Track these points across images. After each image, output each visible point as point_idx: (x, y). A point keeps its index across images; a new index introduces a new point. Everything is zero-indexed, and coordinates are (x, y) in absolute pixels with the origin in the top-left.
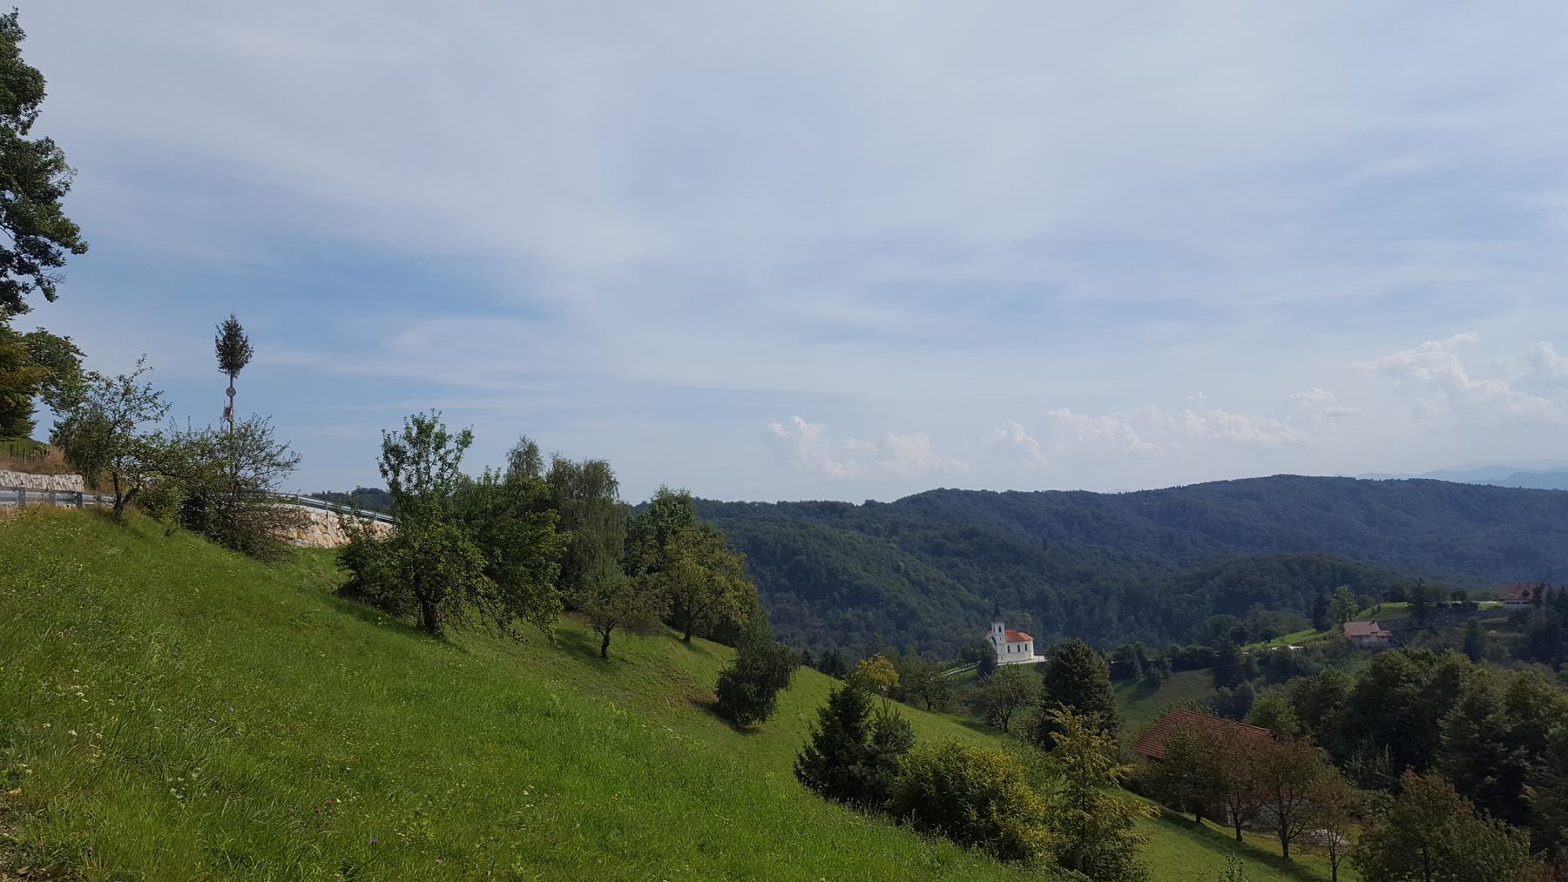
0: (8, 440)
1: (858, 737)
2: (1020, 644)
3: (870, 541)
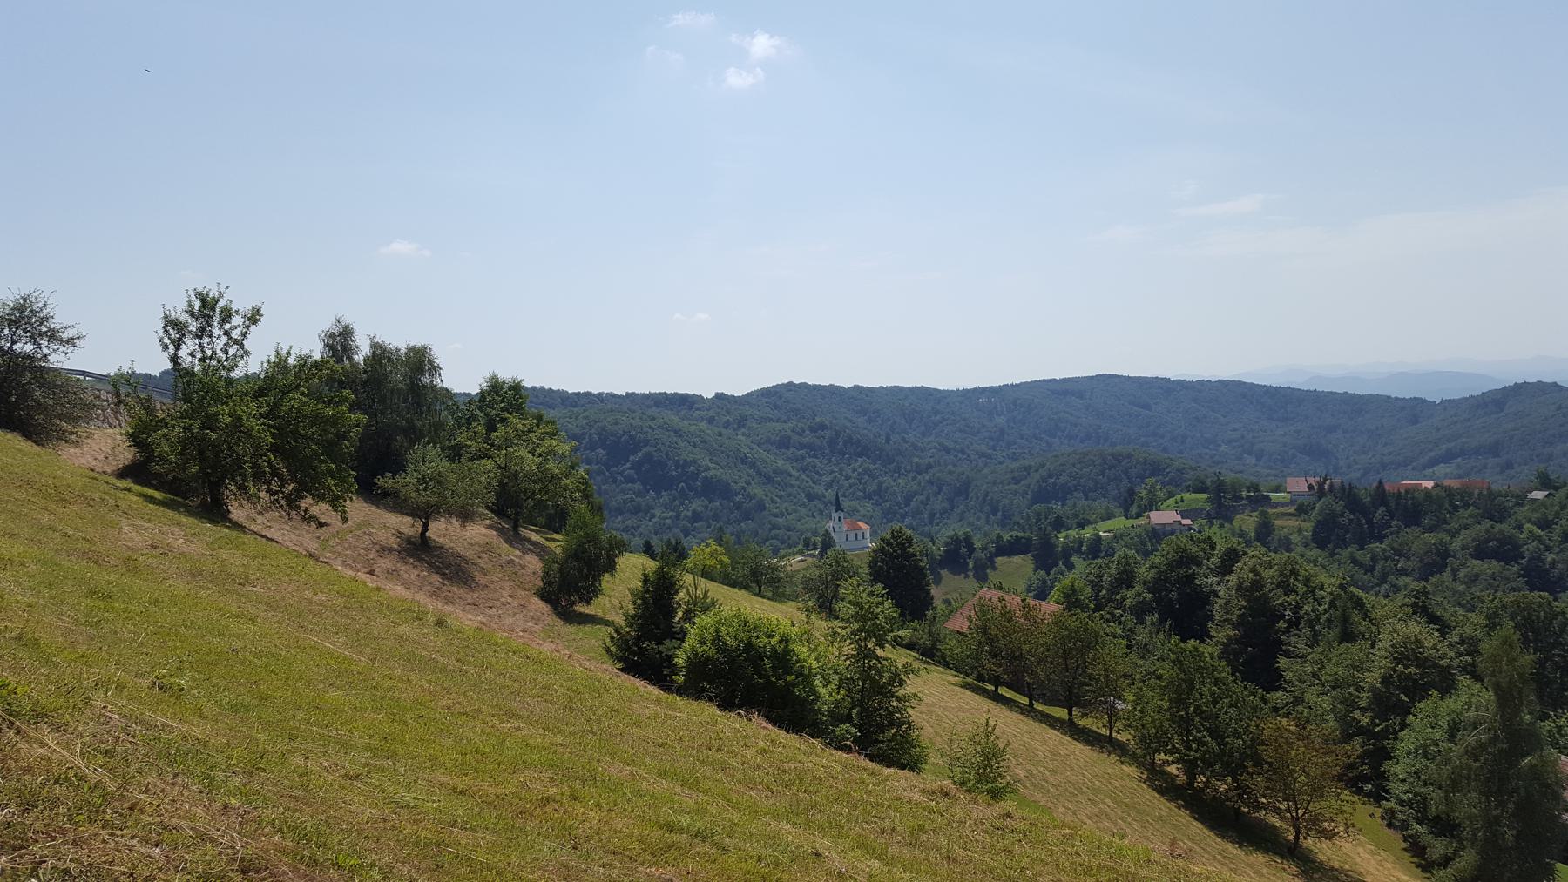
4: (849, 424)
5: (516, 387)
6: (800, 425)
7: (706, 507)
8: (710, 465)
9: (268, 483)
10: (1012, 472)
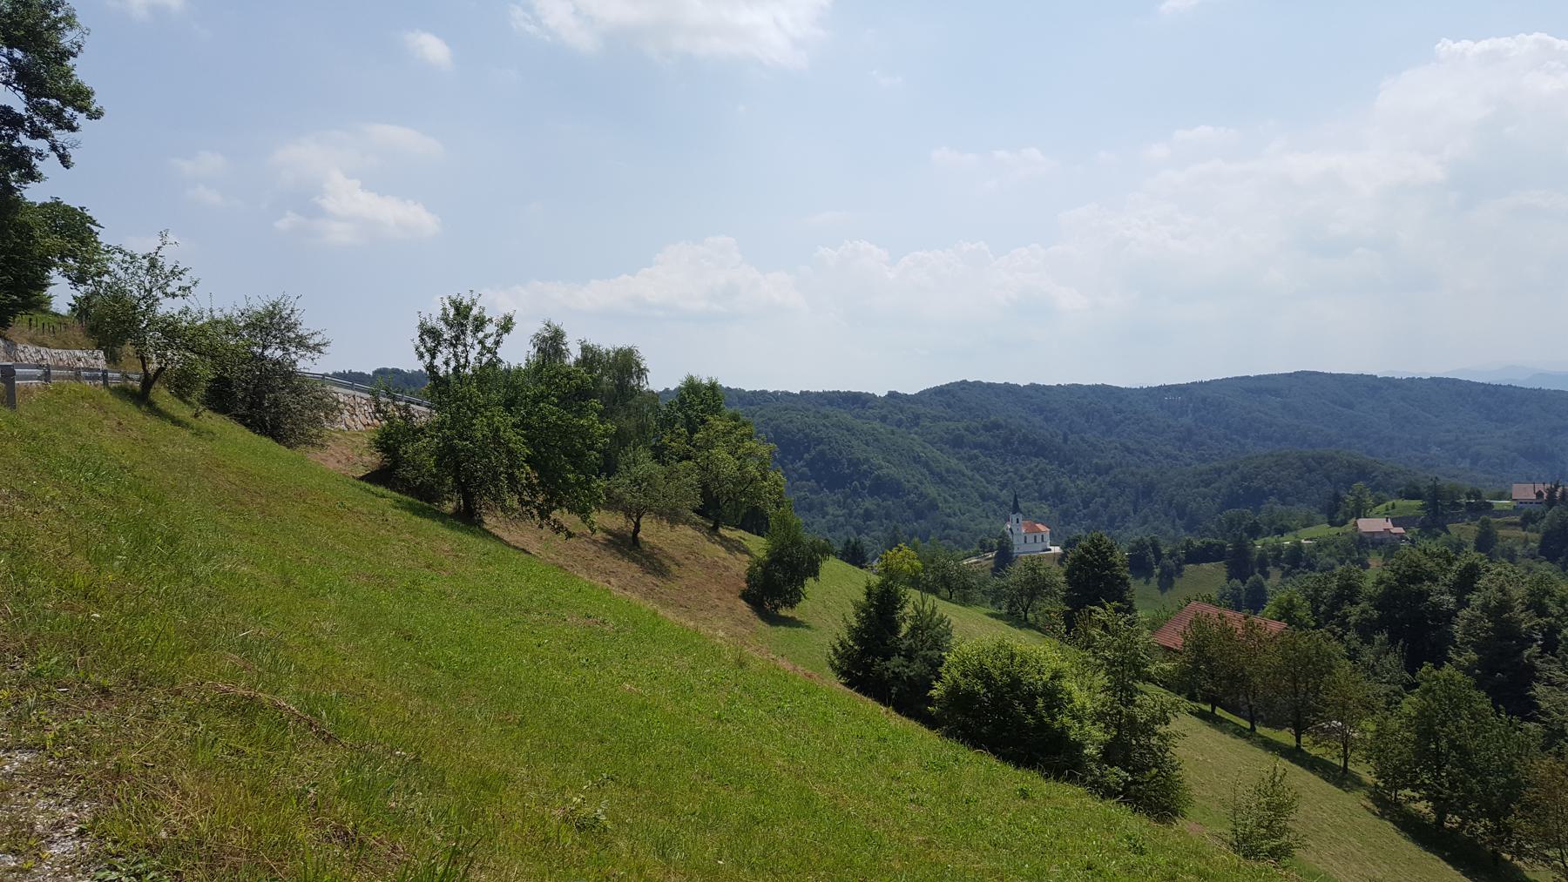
0: (27, 314)
1: (894, 629)
2: (1036, 534)
3: (893, 433)
4: (1025, 424)
5: (713, 387)
6: (974, 424)
7: (878, 505)
8: (883, 463)
9: (520, 494)
10: (1201, 474)
